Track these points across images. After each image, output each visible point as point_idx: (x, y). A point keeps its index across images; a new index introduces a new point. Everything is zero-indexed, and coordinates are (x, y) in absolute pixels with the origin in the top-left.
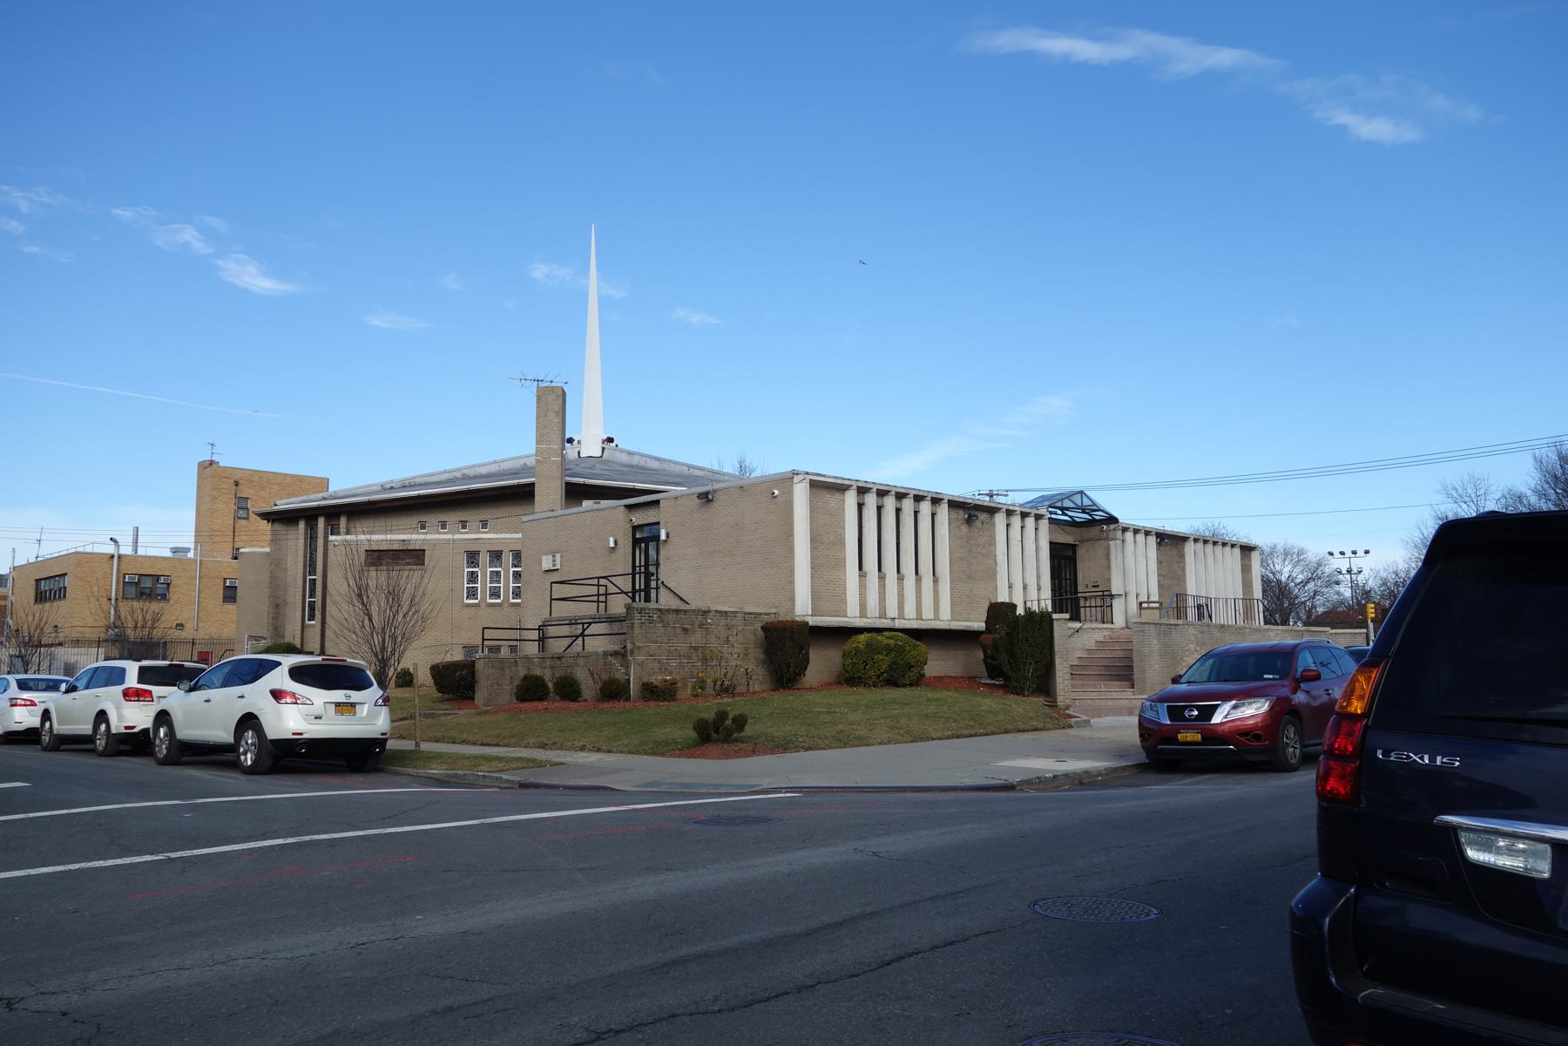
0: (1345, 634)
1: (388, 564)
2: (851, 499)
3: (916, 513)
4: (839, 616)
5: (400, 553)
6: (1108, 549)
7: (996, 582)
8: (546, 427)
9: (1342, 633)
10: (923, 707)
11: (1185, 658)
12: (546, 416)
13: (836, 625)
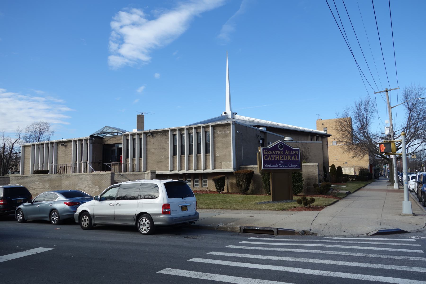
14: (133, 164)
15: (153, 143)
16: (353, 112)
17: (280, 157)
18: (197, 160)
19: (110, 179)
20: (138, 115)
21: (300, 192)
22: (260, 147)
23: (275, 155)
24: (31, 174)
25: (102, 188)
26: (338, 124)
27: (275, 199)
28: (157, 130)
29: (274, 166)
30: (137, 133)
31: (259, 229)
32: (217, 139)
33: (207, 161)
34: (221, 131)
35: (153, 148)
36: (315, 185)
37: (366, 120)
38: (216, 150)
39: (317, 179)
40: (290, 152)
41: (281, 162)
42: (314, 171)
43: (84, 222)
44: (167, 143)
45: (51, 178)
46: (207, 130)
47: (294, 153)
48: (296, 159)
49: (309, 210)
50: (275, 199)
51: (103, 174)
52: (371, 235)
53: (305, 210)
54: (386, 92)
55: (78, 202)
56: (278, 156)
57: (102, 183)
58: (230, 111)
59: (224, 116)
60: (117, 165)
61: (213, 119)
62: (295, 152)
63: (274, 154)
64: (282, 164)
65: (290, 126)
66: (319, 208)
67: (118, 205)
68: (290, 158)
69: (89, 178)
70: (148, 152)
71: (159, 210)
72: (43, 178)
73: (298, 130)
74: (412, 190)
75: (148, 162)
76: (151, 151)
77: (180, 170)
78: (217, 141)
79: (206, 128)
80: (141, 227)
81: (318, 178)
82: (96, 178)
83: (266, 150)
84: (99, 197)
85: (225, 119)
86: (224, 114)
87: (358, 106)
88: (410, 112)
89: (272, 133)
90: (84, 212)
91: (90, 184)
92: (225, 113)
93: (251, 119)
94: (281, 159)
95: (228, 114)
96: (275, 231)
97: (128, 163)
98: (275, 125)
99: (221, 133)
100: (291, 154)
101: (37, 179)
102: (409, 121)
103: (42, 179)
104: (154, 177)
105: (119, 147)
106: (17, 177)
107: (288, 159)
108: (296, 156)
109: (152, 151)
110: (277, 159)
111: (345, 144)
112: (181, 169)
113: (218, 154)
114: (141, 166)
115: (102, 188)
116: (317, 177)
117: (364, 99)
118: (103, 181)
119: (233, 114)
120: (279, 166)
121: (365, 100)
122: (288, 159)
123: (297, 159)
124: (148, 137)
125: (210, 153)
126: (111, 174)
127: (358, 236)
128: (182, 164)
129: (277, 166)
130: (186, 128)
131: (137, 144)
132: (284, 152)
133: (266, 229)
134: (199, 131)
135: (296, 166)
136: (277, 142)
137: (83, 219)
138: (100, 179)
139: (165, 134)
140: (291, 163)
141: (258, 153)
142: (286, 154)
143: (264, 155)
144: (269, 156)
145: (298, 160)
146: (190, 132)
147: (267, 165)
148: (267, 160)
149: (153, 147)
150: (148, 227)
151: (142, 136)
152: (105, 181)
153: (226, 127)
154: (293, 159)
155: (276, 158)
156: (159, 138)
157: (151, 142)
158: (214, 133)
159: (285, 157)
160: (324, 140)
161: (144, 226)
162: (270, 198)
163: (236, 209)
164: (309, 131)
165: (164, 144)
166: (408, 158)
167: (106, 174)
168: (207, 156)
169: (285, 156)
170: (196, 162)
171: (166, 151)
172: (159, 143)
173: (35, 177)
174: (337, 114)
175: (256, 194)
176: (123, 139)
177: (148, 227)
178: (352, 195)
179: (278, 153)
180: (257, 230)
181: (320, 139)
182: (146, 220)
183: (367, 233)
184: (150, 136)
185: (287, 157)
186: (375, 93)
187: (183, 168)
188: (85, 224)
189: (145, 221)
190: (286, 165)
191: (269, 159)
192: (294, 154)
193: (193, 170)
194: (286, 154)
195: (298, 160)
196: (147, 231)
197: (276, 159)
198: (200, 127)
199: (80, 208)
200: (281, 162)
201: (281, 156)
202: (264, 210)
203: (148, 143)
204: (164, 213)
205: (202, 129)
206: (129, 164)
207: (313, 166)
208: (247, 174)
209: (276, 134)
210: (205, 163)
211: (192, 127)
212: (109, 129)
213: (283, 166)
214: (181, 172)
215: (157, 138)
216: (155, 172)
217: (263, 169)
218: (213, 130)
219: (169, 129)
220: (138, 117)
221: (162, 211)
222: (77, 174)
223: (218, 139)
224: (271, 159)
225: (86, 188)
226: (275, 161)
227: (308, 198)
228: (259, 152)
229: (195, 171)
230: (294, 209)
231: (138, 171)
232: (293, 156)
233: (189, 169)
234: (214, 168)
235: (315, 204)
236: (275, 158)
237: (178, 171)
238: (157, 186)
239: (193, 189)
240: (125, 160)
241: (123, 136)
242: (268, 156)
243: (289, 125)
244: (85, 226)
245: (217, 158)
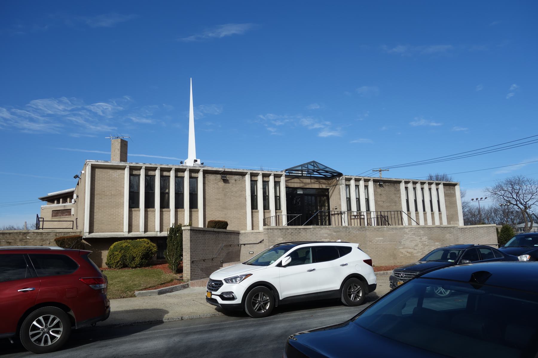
0: (483, 227)
1: (60, 215)
2: (248, 178)
3: (437, 189)
4: (118, 232)
5: (64, 211)
6: (339, 189)
7: (246, 210)
8: (115, 156)
9: (481, 227)
10: (114, 283)
11: (403, 242)
12: (115, 151)
13: (109, 236)
24: (207, 227)
34: (447, 191)
45: (349, 232)
46: (151, 173)
69: (422, 232)
72: (335, 232)
91: (425, 240)
101: (326, 233)
103: (335, 234)
105: (298, 193)
106: (284, 230)
152: (450, 236)
166: (498, 223)
167: (451, 227)
168: (164, 212)
173: (322, 230)
219: (402, 180)
222: (327, 226)
225: (418, 246)
234: (130, 231)
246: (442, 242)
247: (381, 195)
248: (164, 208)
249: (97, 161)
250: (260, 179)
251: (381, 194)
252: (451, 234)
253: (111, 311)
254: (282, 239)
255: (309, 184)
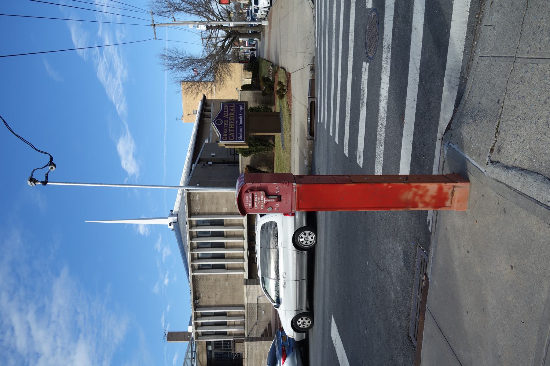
14: (235, 325)
15: (209, 297)
16: (176, 74)
17: (231, 124)
18: (231, 237)
19: (254, 343)
20: (168, 341)
21: (271, 110)
22: (219, 144)
23: (228, 128)
25: (264, 355)
26: (190, 92)
27: (279, 130)
28: (192, 291)
29: (241, 130)
30: (195, 320)
31: (309, 118)
32: (206, 210)
33: (234, 223)
34: (197, 206)
35: (215, 297)
36: (264, 94)
37: (186, 59)
38: (219, 212)
39: (257, 92)
40: (226, 113)
41: (237, 122)
42: (247, 95)
43: (305, 324)
44: (209, 278)
46: (194, 223)
47: (226, 109)
48: (234, 107)
49: (290, 86)
50: (279, 130)
51: (247, 353)
52: (313, 4)
53: (290, 90)
54: (155, 26)
55: (282, 347)
56: (230, 125)
57: (259, 355)
58: (168, 218)
59: (174, 225)
60: (235, 345)
61: (177, 238)
62: (226, 107)
63: (227, 129)
64: (239, 121)
65: (191, 144)
66: (288, 76)
67: (285, 276)
68: (232, 113)
70: (220, 303)
71: (290, 220)
73: (195, 135)
74: (269, 5)
75: (232, 304)
76: (218, 300)
77: (243, 259)
78: (208, 210)
79: (192, 225)
80: (309, 243)
81: (256, 92)
82: (252, 364)
83: (223, 137)
84: (275, 304)
85: (179, 224)
86: (172, 227)
87: (169, 67)
88: (179, 9)
89: (200, 152)
90: (294, 325)
92: (170, 225)
93: (180, 192)
94: (234, 123)
95: (172, 221)
96: (311, 100)
97: (233, 333)
98: (189, 161)
99: (199, 205)
100: (227, 111)
102: (189, 12)
104: (252, 281)
107: (233, 116)
108: (230, 107)
109: (218, 299)
110: (233, 126)
111: (215, 85)
112: (242, 258)
113: (225, 210)
114: (237, 313)
115: (264, 355)
116: (255, 92)
117: (161, 60)
118: (256, 352)
119: (172, 215)
120: (241, 125)
121: (161, 59)
122: (233, 115)
123: (233, 105)
124: (200, 304)
125: (223, 220)
126: (247, 341)
127: (314, 17)
128: (237, 257)
129: (241, 127)
130: (191, 251)
131: (208, 320)
132: (225, 119)
133: (309, 111)
134: (195, 234)
135: (241, 107)
136: (214, 125)
137: (302, 326)
138: (254, 358)
139: (197, 280)
140: (238, 113)
141: (227, 147)
142: (227, 117)
143: (228, 140)
144: (230, 134)
145: (234, 105)
146: (196, 246)
147: (241, 138)
148: (234, 137)
149: (214, 297)
150: (309, 234)
151: (199, 313)
152: (257, 350)
153: (191, 199)
154: (234, 110)
155: (232, 127)
156: (201, 290)
157: (206, 301)
158: (199, 214)
159: (231, 118)
160: (209, 103)
161: (308, 239)
162: (277, 136)
163: (290, 169)
164: (198, 120)
165: (210, 282)
167: (247, 348)
168: (228, 223)
169: (230, 118)
170: (234, 238)
171: (219, 280)
172: (208, 289)
174: (178, 92)
175: (273, 163)
176: (201, 340)
177: (308, 234)
178: (274, 61)
179: (226, 126)
180: (311, 120)
181: (207, 108)
182: (302, 238)
183: (311, 9)
184: (199, 302)
185: (231, 116)
186: (156, 38)
187: (241, 255)
188: (307, 323)
189: (303, 239)
190: (241, 117)
191: (233, 134)
192: (228, 109)
193: (243, 242)
194: (227, 117)
195: (234, 105)
196: (313, 235)
197: (234, 127)
198: (190, 232)
199: (289, 332)
200: (237, 122)
201: (230, 123)
202: (290, 136)
203: (208, 304)
204: (293, 215)
205: (192, 230)
206: (235, 330)
207: (241, 96)
208: (250, 172)
209: (202, 150)
210: (236, 226)
211: (190, 243)
212: (186, 362)
213: (241, 120)
214: (246, 258)
215: (202, 292)
216: (246, 279)
217: (245, 141)
218: (194, 215)
220: (170, 341)
221: (291, 216)
223: (207, 209)
224: (234, 133)
226: (235, 129)
227: (277, 88)
228: (225, 146)
229: (245, 240)
230: (289, 104)
231: (243, 317)
232: (231, 110)
233: (242, 248)
235: (283, 81)
236: (232, 129)
237: (245, 261)
238: (264, 225)
239: (267, 76)
240: (229, 337)
241: (198, 340)
242: (230, 136)
243: (189, 148)
244: (309, 322)
245: (229, 211)
246: (262, 357)
247: (209, 297)
248: (223, 223)
249: (194, 358)
250: (200, 321)
251: (208, 297)
252: (254, 349)
253: (298, 174)
254: (243, 47)
255: (202, 347)
